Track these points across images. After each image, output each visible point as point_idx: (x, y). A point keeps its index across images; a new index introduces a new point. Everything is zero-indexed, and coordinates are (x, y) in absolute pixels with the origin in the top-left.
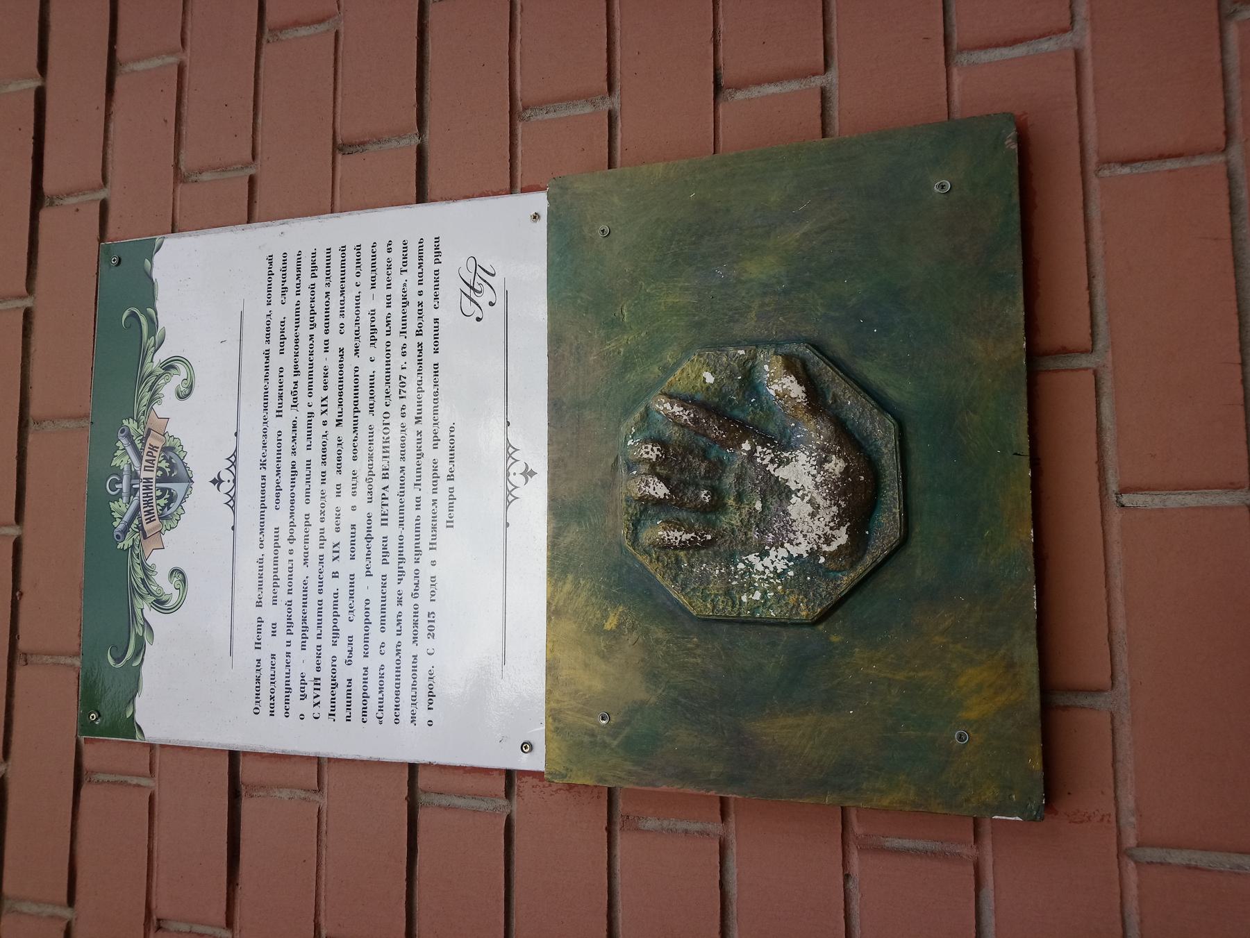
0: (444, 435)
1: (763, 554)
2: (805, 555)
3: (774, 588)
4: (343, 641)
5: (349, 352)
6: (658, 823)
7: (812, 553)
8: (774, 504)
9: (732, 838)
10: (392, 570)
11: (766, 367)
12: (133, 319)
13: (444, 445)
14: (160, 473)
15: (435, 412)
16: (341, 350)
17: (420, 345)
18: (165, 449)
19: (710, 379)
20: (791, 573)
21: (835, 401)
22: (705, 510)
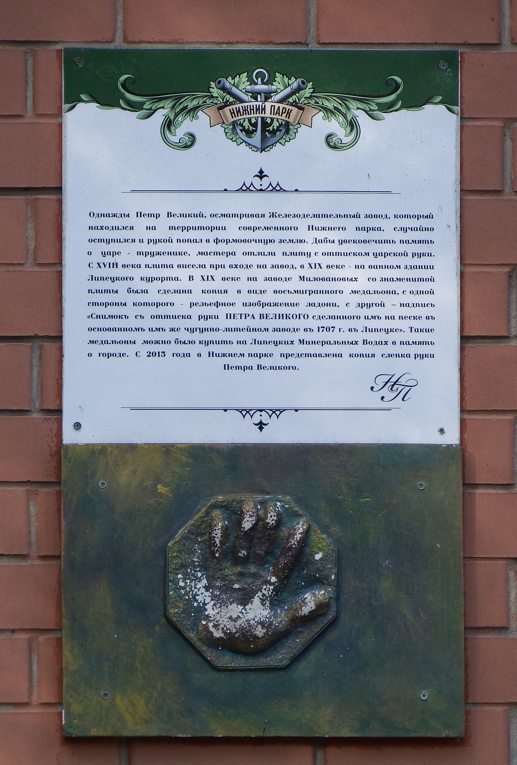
0: (290, 362)
1: (207, 588)
2: (207, 613)
3: (187, 593)
4: (144, 285)
5: (354, 286)
6: (34, 514)
7: (207, 617)
8: (239, 595)
9: (29, 562)
10: (194, 323)
11: (323, 592)
12: (393, 86)
13: (284, 362)
14: (269, 121)
15: (308, 355)
16: (356, 279)
17: (356, 343)
18: (287, 124)
19: (318, 557)
20: (195, 604)
21: (299, 632)
22: (234, 551)
